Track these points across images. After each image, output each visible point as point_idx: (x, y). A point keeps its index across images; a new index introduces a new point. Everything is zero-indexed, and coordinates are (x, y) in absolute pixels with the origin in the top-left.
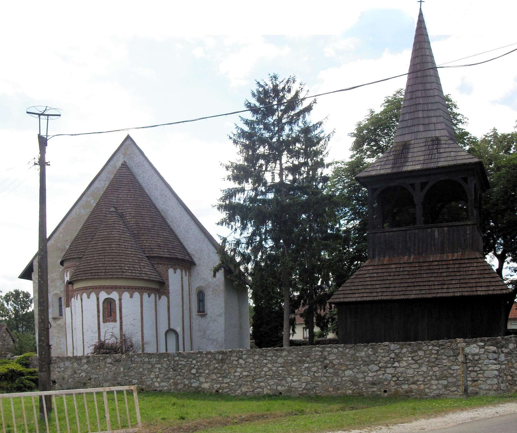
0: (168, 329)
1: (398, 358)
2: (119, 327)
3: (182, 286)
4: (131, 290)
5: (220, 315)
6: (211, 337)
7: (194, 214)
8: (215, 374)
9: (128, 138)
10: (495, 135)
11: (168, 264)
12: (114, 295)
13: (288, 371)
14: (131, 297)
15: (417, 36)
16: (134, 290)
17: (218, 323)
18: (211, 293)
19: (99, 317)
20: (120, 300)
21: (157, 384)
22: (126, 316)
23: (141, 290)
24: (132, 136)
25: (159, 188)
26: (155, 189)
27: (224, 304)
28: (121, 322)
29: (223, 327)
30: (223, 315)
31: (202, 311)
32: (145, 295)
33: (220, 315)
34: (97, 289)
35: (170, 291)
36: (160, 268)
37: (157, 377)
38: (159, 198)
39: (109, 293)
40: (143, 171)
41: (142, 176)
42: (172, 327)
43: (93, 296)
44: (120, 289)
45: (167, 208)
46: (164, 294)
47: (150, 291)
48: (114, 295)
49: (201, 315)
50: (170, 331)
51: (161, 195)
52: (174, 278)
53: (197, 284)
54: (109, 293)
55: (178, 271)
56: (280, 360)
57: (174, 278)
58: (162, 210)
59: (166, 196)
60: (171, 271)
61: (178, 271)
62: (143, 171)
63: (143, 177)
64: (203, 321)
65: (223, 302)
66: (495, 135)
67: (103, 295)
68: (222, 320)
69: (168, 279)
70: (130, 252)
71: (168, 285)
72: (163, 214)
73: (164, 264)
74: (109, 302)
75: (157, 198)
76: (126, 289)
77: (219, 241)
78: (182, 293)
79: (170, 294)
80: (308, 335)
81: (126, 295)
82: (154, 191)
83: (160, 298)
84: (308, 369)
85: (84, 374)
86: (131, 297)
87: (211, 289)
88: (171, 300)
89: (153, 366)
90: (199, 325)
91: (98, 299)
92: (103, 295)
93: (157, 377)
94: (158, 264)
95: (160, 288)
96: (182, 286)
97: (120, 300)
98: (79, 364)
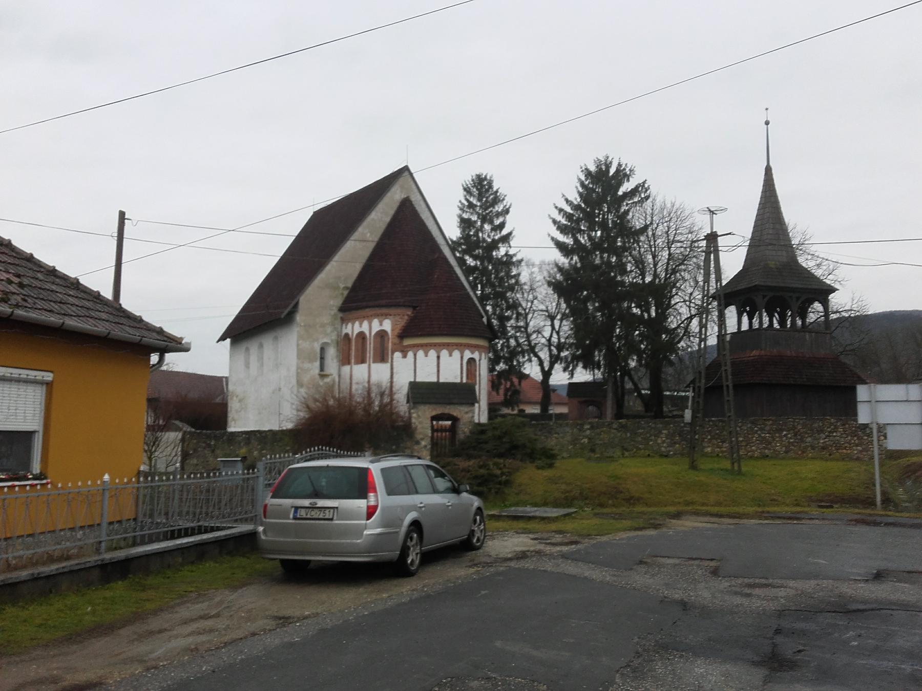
1: (836, 429)
8: (716, 439)
10: (588, 174)
12: (476, 355)
13: (772, 437)
14: (451, 355)
15: (766, 174)
21: (663, 449)
32: (421, 353)
34: (461, 347)
37: (664, 442)
43: (457, 354)
48: (476, 355)
54: (473, 353)
56: (767, 428)
66: (588, 174)
67: (468, 354)
84: (785, 435)
85: (586, 440)
86: (451, 355)
89: (660, 432)
91: (462, 358)
92: (468, 354)
93: (664, 442)
98: (580, 430)
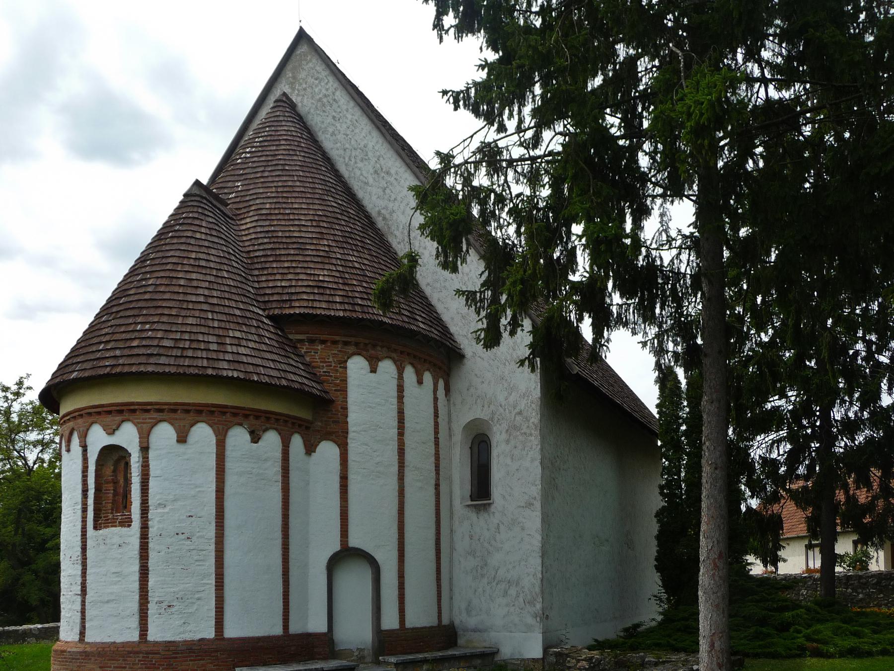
0: (337, 547)
2: (135, 542)
3: (401, 413)
4: (183, 417)
5: (529, 505)
6: (501, 572)
7: (643, 401)
9: (302, 37)
11: (346, 343)
12: (127, 436)
14: (182, 439)
16: (190, 417)
17: (523, 529)
18: (504, 436)
19: (84, 510)
20: (145, 449)
22: (162, 505)
23: (221, 419)
24: (308, 31)
25: (370, 154)
26: (362, 161)
27: (539, 470)
28: (145, 527)
29: (536, 541)
30: (538, 505)
31: (481, 489)
32: (238, 437)
33: (529, 505)
35: (351, 428)
36: (318, 355)
38: (371, 181)
39: (111, 432)
40: (334, 117)
41: (331, 130)
42: (354, 541)
44: (146, 415)
45: (391, 205)
46: (327, 436)
47: (287, 426)
49: (475, 506)
50: (346, 555)
51: (376, 172)
52: (369, 387)
53: (466, 413)
54: (111, 432)
55: (387, 367)
57: (369, 387)
58: (379, 213)
59: (388, 173)
60: (357, 366)
61: (387, 367)
62: (334, 117)
63: (333, 134)
64: (481, 524)
65: (537, 463)
67: (98, 438)
68: (533, 520)
69: (344, 390)
70: (202, 299)
71: (345, 408)
72: (380, 224)
73: (335, 342)
74: (113, 455)
75: (367, 184)
76: (126, 416)
77: (434, 164)
78: (401, 434)
79: (351, 435)
80: (818, 564)
81: (164, 434)
82: (360, 165)
83: (310, 449)
87: (505, 426)
88: (351, 456)
90: (471, 537)
92: (98, 438)
94: (312, 341)
95: (317, 415)
96: (401, 413)
97: (145, 449)
